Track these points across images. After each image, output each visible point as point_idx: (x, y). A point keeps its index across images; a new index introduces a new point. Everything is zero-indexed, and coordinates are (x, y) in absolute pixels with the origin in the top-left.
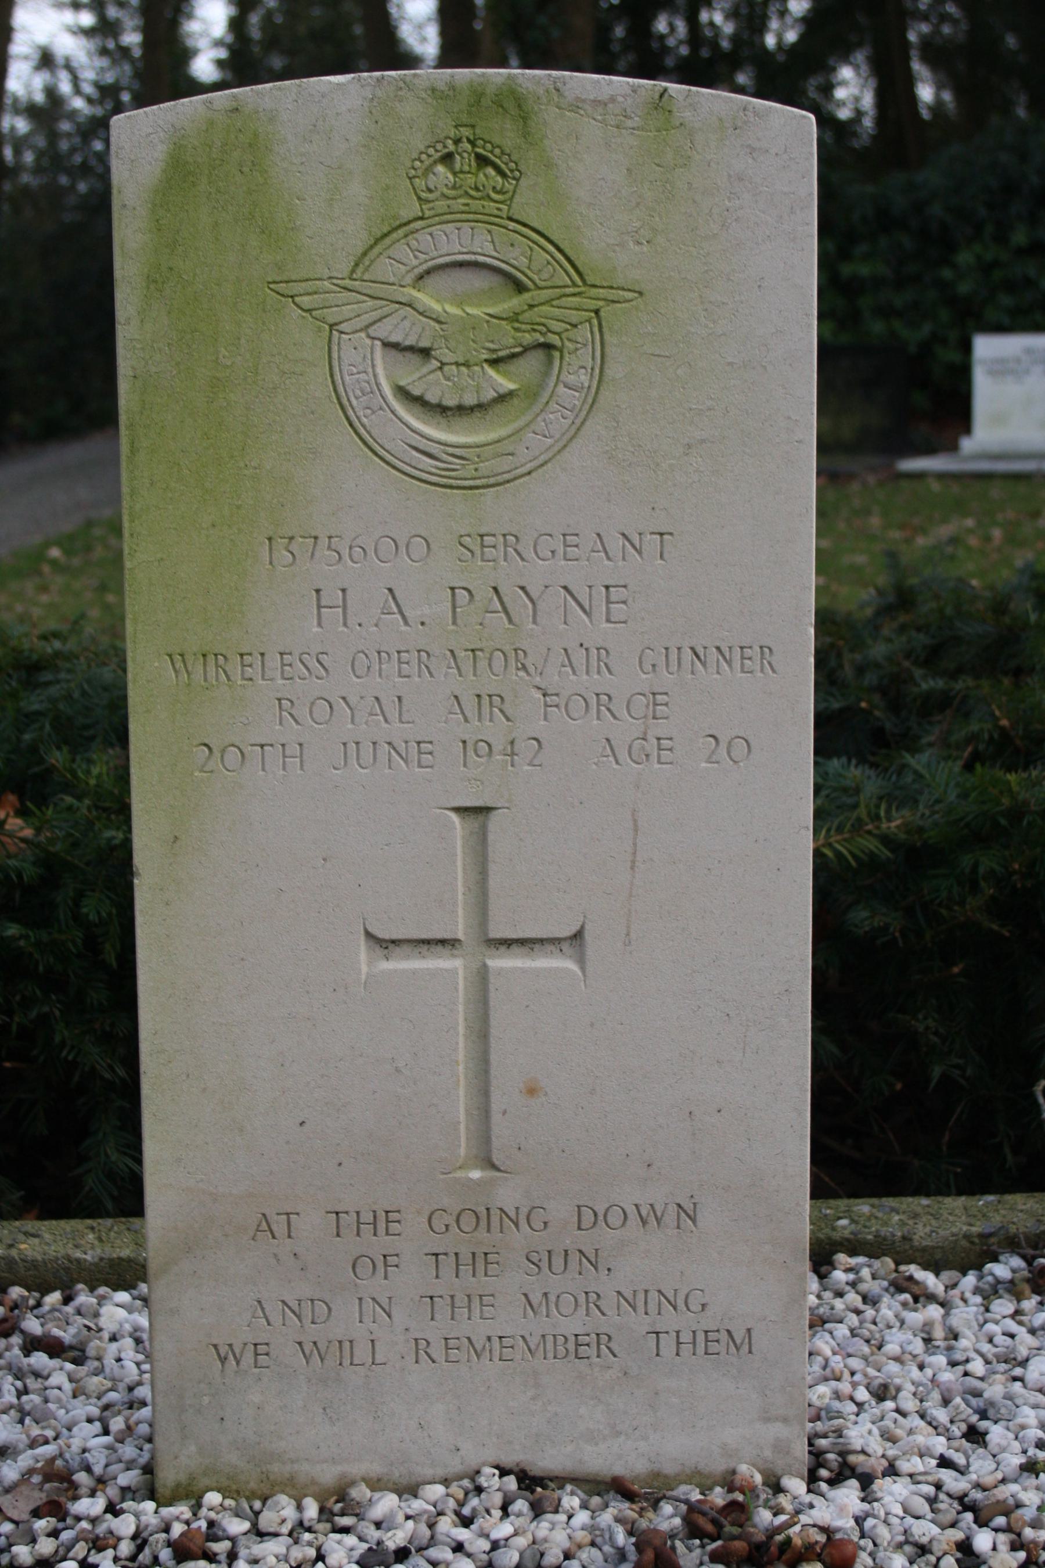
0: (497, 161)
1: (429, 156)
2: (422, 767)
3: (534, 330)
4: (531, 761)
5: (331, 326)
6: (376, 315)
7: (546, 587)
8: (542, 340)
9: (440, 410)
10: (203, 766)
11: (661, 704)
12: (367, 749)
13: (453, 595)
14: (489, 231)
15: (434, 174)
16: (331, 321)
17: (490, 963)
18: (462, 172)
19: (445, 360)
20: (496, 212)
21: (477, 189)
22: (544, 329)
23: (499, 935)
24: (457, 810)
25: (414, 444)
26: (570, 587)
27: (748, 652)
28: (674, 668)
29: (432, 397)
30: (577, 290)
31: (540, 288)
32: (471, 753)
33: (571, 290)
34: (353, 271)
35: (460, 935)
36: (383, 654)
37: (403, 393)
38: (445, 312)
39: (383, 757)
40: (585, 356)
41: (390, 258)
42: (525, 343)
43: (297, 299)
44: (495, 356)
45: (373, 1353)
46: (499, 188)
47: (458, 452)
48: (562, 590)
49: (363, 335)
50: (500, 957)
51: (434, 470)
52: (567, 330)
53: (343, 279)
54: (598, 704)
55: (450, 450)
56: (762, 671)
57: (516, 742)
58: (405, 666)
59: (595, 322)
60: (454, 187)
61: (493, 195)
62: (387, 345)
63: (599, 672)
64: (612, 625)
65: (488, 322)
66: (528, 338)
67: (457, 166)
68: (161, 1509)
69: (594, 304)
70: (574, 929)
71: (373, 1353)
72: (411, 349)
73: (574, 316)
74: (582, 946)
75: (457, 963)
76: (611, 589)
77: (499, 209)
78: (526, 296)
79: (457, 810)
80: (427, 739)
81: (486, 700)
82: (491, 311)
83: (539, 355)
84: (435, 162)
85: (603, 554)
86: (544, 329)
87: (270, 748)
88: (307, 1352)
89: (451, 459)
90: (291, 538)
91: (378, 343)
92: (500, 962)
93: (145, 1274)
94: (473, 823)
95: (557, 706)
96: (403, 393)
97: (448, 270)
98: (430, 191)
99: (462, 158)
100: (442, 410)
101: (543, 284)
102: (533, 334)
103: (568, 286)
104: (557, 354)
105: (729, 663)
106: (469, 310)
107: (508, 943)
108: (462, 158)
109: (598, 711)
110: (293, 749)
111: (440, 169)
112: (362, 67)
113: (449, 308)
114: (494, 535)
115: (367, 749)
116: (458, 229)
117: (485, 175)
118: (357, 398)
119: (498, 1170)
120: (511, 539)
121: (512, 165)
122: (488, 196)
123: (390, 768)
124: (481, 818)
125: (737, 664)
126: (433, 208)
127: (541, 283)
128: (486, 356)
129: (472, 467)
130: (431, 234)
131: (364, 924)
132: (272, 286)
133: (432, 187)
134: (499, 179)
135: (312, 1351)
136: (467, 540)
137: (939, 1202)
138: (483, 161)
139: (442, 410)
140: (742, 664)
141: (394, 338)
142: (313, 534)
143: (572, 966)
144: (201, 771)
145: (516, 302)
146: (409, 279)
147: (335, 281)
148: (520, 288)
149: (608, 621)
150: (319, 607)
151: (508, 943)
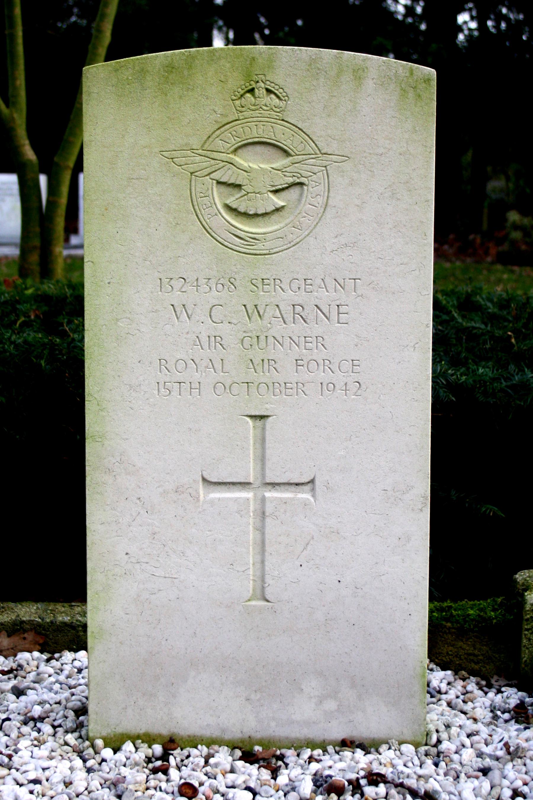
0: (276, 91)
3: (294, 176)
5: (192, 173)
7: (266, 305)
8: (298, 181)
10: (356, 393)
13: (294, 308)
14: (272, 127)
15: (244, 98)
16: (192, 171)
18: (259, 97)
19: (249, 191)
20: (276, 117)
21: (266, 106)
23: (268, 482)
24: (251, 417)
26: (319, 306)
29: (242, 209)
30: (316, 156)
31: (297, 155)
32: (325, 387)
37: (229, 208)
38: (249, 167)
40: (321, 189)
41: (221, 140)
42: (289, 183)
43: (174, 160)
44: (274, 189)
46: (253, 103)
48: (315, 307)
49: (208, 177)
50: (213, 492)
53: (197, 150)
57: (348, 384)
59: (325, 171)
60: (254, 105)
62: (219, 183)
64: (340, 325)
65: (270, 172)
66: (291, 180)
68: (419, 749)
69: (325, 163)
70: (312, 478)
73: (316, 169)
76: (340, 307)
77: (278, 116)
78: (291, 158)
79: (251, 417)
81: (266, 361)
82: (274, 166)
85: (324, 289)
86: (299, 176)
89: (251, 240)
91: (215, 182)
92: (269, 494)
93: (86, 643)
94: (259, 423)
95: (302, 366)
96: (229, 208)
98: (243, 107)
99: (259, 90)
100: (245, 215)
101: (299, 153)
102: (294, 178)
103: (313, 154)
104: (305, 187)
107: (274, 485)
111: (248, 95)
112: (430, 60)
116: (256, 125)
117: (270, 98)
119: (268, 601)
121: (284, 94)
124: (262, 420)
126: (243, 116)
132: (161, 153)
133: (243, 105)
134: (277, 100)
136: (254, 281)
138: (269, 91)
139: (245, 215)
143: (312, 499)
145: (287, 161)
148: (286, 154)
149: (339, 323)
151: (274, 485)
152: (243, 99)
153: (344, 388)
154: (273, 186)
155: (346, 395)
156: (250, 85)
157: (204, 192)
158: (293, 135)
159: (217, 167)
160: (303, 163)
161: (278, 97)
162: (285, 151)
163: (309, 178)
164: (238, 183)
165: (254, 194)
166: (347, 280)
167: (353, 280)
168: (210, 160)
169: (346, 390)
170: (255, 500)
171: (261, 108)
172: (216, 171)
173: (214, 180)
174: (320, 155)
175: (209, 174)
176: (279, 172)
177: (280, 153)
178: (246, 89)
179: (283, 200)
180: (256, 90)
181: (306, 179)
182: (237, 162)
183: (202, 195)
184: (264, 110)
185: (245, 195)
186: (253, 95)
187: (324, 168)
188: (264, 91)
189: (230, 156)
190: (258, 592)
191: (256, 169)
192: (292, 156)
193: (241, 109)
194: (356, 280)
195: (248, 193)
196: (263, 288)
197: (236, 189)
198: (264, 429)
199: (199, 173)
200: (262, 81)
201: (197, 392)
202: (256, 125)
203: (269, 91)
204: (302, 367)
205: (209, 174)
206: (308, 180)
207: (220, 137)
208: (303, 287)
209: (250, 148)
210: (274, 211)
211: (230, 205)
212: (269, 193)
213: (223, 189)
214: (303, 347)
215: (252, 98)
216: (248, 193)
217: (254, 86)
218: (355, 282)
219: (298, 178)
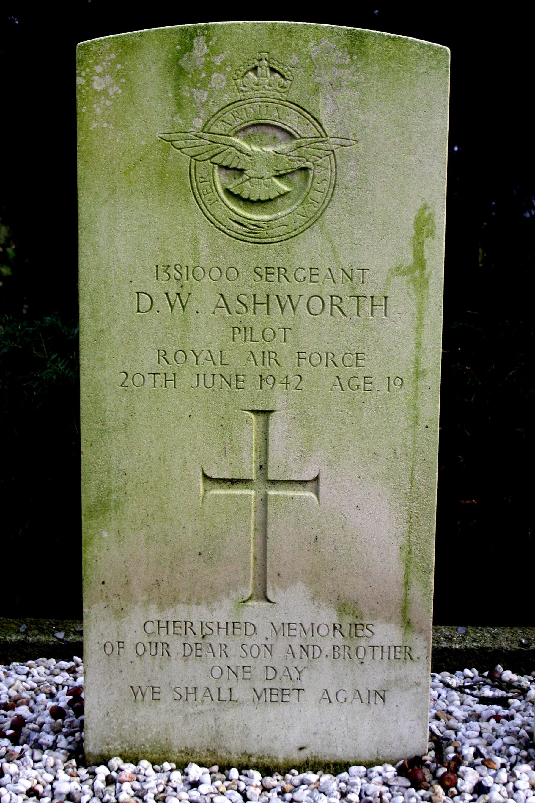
0: (281, 71)
4: (296, 387)
5: (192, 157)
6: (216, 151)
7: (300, 296)
8: (303, 166)
9: (248, 202)
17: (270, 493)
19: (251, 176)
21: (270, 86)
24: (252, 411)
30: (324, 139)
31: (303, 138)
32: (392, 382)
33: (320, 139)
34: (204, 127)
37: (228, 192)
38: (252, 150)
44: (278, 174)
45: (231, 696)
49: (209, 161)
54: (327, 358)
55: (253, 222)
59: (332, 155)
61: (279, 89)
62: (221, 167)
65: (274, 156)
71: (231, 696)
72: (235, 169)
74: (318, 483)
75: (253, 493)
76: (334, 297)
78: (295, 141)
81: (267, 355)
82: (277, 149)
87: (158, 375)
88: (135, 691)
90: (168, 266)
94: (261, 418)
95: (305, 359)
96: (228, 192)
99: (262, 69)
106: (265, 149)
107: (274, 482)
108: (262, 69)
110: (170, 376)
111: (251, 74)
118: (204, 195)
120: (283, 271)
122: (252, 88)
123: (389, 390)
127: (303, 135)
129: (265, 232)
130: (245, 109)
131: (203, 470)
135: (138, 691)
136: (258, 270)
141: (225, 164)
142: (168, 264)
143: (314, 496)
144: (296, 388)
146: (232, 133)
148: (291, 136)
153: (285, 381)
154: (278, 171)
155: (286, 388)
157: (204, 176)
158: (280, 118)
161: (283, 76)
165: (257, 179)
167: (361, 271)
169: (287, 383)
170: (255, 498)
171: (264, 87)
172: (216, 155)
173: (216, 164)
177: (279, 135)
180: (259, 69)
182: (237, 143)
183: (203, 180)
184: (268, 90)
186: (256, 75)
187: (331, 152)
188: (268, 69)
190: (261, 594)
195: (251, 178)
196: (266, 277)
198: (267, 420)
199: (199, 156)
200: (266, 60)
202: (260, 106)
203: (273, 70)
207: (222, 118)
210: (276, 198)
211: (231, 190)
212: (273, 179)
213: (224, 172)
215: (255, 77)
216: (251, 178)
217: (257, 63)
219: (304, 162)
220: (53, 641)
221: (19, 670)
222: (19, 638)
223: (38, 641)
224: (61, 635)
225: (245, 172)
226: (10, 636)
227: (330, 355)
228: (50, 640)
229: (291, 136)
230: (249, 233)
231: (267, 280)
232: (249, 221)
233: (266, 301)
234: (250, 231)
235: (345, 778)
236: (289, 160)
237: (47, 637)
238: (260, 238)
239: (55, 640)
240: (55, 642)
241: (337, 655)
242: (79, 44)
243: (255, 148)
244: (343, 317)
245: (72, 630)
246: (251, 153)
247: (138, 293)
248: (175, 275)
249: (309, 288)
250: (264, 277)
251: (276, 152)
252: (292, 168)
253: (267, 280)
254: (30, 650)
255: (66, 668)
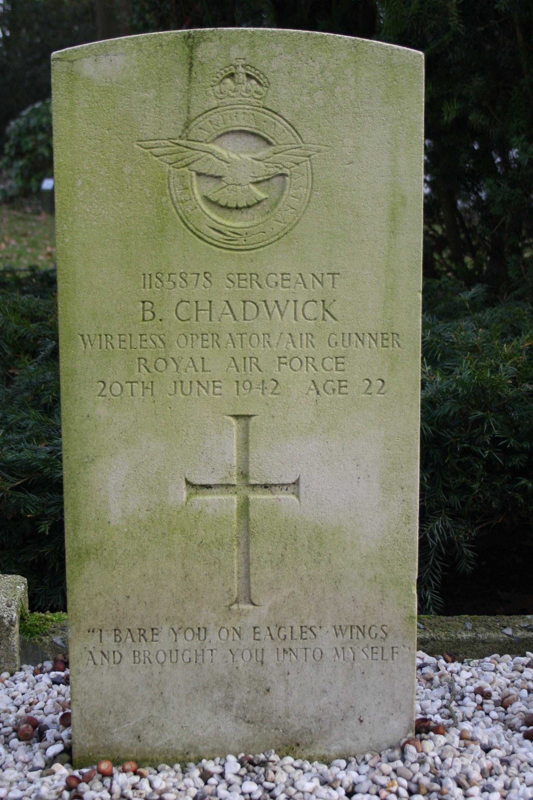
0: (257, 77)
1: (222, 75)
2: (215, 395)
4: (101, 393)
8: (280, 172)
11: (283, 364)
12: (187, 385)
17: (252, 497)
22: (281, 166)
25: (213, 227)
27: (123, 337)
28: (346, 343)
29: (223, 203)
32: (241, 387)
35: (235, 482)
36: (215, 336)
37: (207, 199)
39: (195, 390)
44: (255, 180)
47: (237, 231)
49: (186, 169)
51: (222, 241)
52: (293, 167)
55: (231, 230)
56: (393, 346)
58: (144, 342)
60: (234, 91)
62: (199, 174)
63: (307, 347)
66: (273, 171)
67: (236, 80)
75: (235, 498)
77: (259, 103)
78: (271, 148)
80: (135, 381)
81: (248, 360)
82: (259, 155)
83: (280, 179)
84: (224, 78)
86: (281, 166)
91: (194, 174)
94: (242, 421)
96: (207, 199)
97: (242, 135)
98: (222, 93)
103: (294, 144)
104: (287, 179)
105: (376, 341)
109: (307, 366)
111: (228, 81)
113: (234, 156)
114: (245, 274)
115: (187, 385)
122: (253, 96)
125: (380, 341)
128: (251, 180)
133: (223, 91)
136: (231, 276)
137: (523, 618)
140: (382, 343)
143: (296, 500)
147: (172, 141)
148: (269, 143)
150: (197, 310)
152: (222, 84)
156: (230, 70)
159: (196, 157)
160: (285, 152)
162: (265, 139)
163: (292, 169)
164: (218, 174)
166: (326, 276)
168: (185, 149)
171: (241, 94)
174: (302, 145)
175: (188, 165)
176: (260, 163)
177: (263, 143)
178: (225, 74)
179: (264, 191)
180: (236, 76)
181: (288, 170)
185: (225, 187)
187: (308, 159)
188: (245, 75)
189: (209, 145)
191: (236, 160)
192: (274, 146)
193: (220, 96)
194: (133, 384)
196: (239, 283)
197: (213, 205)
198: (247, 426)
201: (206, 314)
203: (248, 76)
204: (285, 365)
205: (188, 165)
206: (290, 171)
208: (280, 283)
209: (251, 139)
213: (202, 178)
214: (381, 345)
216: (228, 184)
218: (132, 386)
219: (281, 169)
220: (503, 637)
221: (485, 666)
222: (469, 635)
223: (489, 638)
224: (509, 631)
225: (223, 179)
226: (460, 633)
227: (310, 360)
228: (501, 636)
229: (269, 143)
230: (223, 239)
231: (239, 287)
232: (228, 228)
233: (208, 308)
234: (229, 238)
235: (24, 786)
236: (267, 166)
237: (496, 633)
238: (238, 245)
239: (506, 636)
240: (505, 638)
241: (137, 659)
242: (54, 53)
243: (234, 156)
244: (335, 322)
245: (517, 626)
246: (229, 160)
247: (244, 302)
248: (204, 283)
249: (281, 294)
250: (237, 284)
251: (254, 159)
252: (269, 175)
253: (239, 287)
254: (481, 646)
255: (526, 664)
